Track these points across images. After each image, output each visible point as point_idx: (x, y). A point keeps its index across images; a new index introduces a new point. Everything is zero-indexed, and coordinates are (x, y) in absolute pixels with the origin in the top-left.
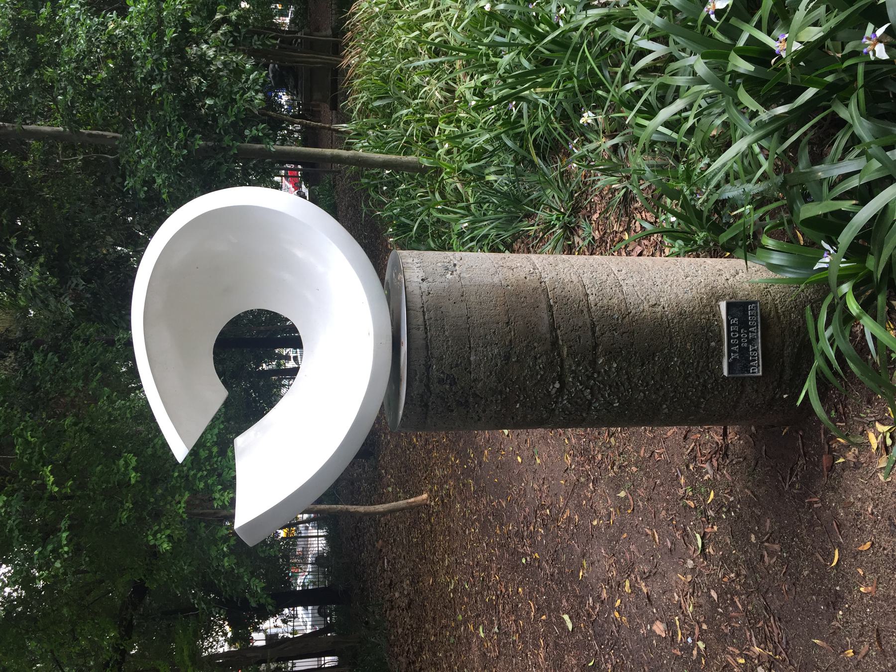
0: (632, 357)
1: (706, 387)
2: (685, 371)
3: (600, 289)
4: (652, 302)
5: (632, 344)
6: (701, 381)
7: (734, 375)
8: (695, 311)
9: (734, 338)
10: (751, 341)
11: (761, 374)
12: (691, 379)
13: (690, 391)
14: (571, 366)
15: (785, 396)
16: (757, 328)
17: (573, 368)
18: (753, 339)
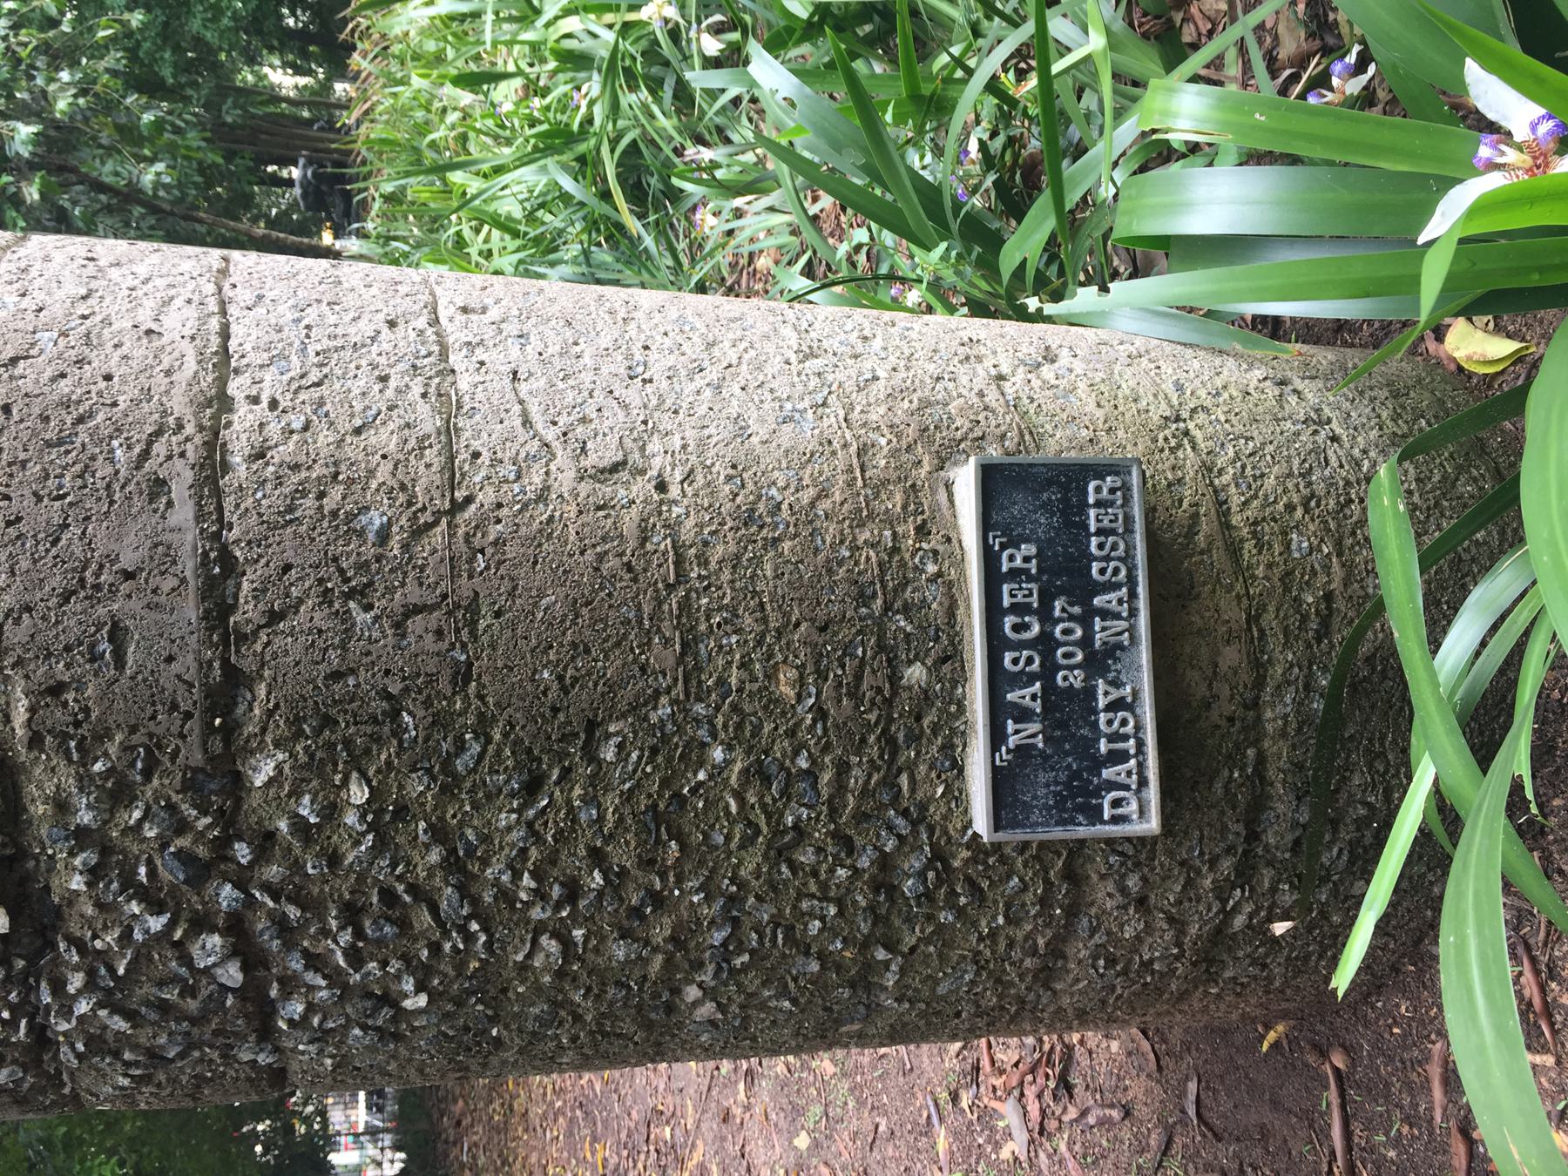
0: (461, 746)
1: (893, 891)
2: (773, 816)
3: (314, 376)
4: (602, 453)
5: (462, 675)
6: (864, 862)
7: (1019, 835)
8: (826, 505)
9: (1071, 668)
10: (1099, 661)
11: (1153, 824)
12: (806, 857)
13: (812, 915)
14: (62, 806)
15: (1280, 928)
16: (1133, 595)
17: (85, 817)
18: (1113, 650)
